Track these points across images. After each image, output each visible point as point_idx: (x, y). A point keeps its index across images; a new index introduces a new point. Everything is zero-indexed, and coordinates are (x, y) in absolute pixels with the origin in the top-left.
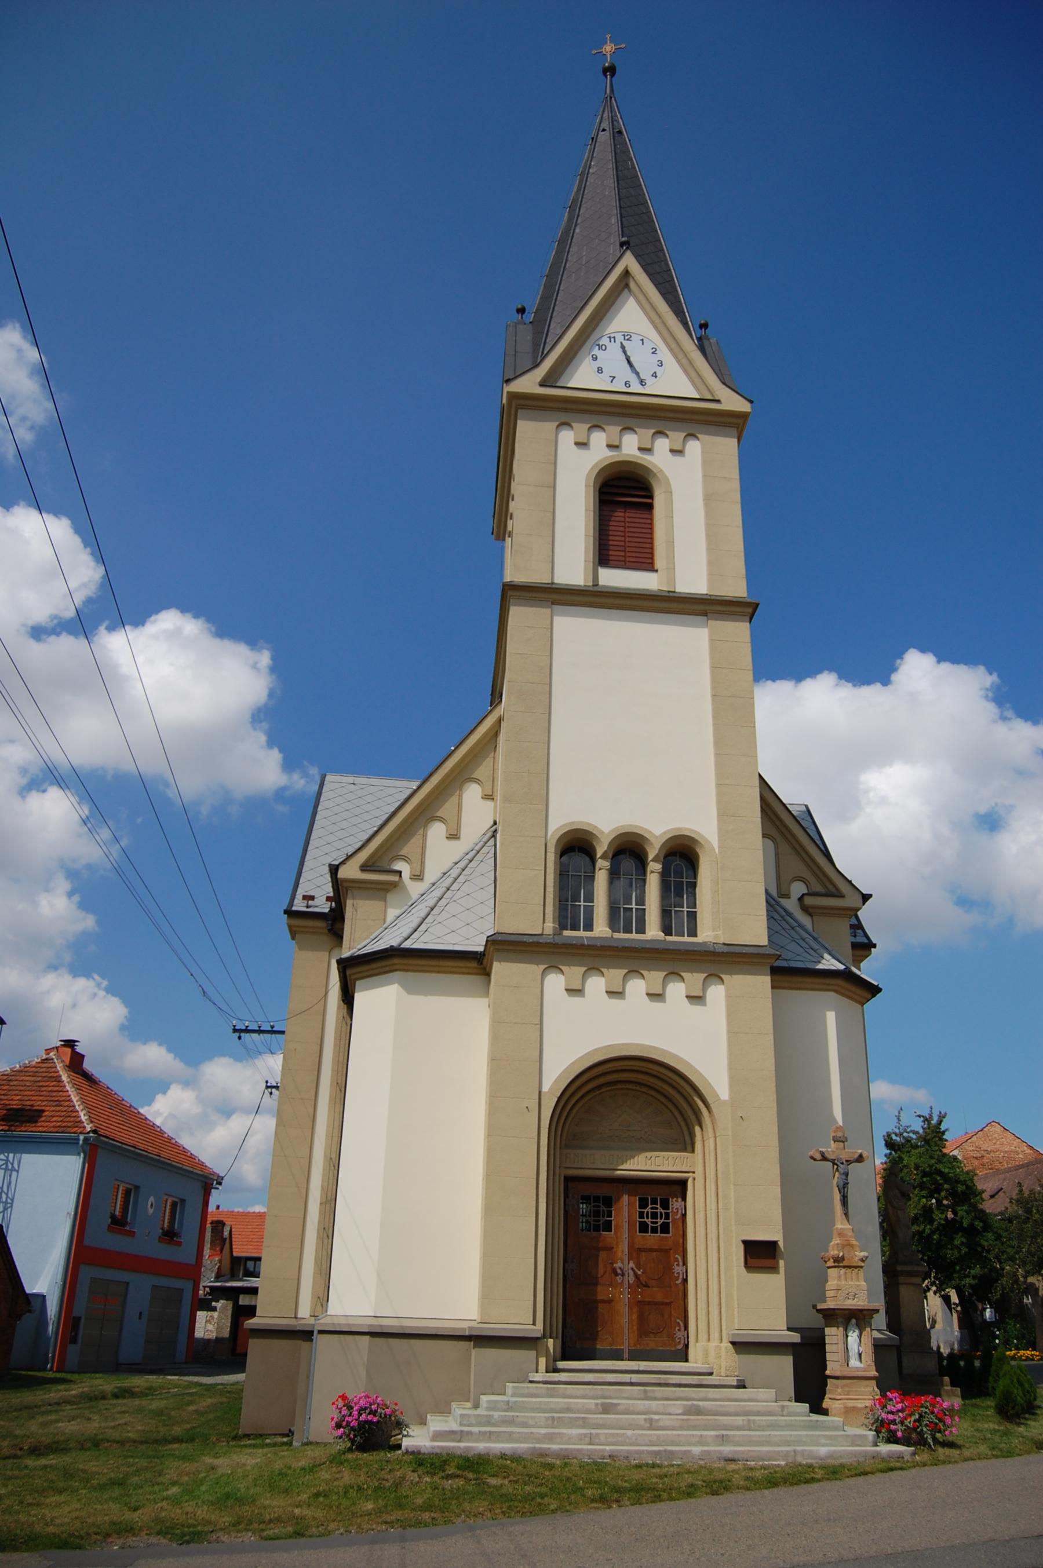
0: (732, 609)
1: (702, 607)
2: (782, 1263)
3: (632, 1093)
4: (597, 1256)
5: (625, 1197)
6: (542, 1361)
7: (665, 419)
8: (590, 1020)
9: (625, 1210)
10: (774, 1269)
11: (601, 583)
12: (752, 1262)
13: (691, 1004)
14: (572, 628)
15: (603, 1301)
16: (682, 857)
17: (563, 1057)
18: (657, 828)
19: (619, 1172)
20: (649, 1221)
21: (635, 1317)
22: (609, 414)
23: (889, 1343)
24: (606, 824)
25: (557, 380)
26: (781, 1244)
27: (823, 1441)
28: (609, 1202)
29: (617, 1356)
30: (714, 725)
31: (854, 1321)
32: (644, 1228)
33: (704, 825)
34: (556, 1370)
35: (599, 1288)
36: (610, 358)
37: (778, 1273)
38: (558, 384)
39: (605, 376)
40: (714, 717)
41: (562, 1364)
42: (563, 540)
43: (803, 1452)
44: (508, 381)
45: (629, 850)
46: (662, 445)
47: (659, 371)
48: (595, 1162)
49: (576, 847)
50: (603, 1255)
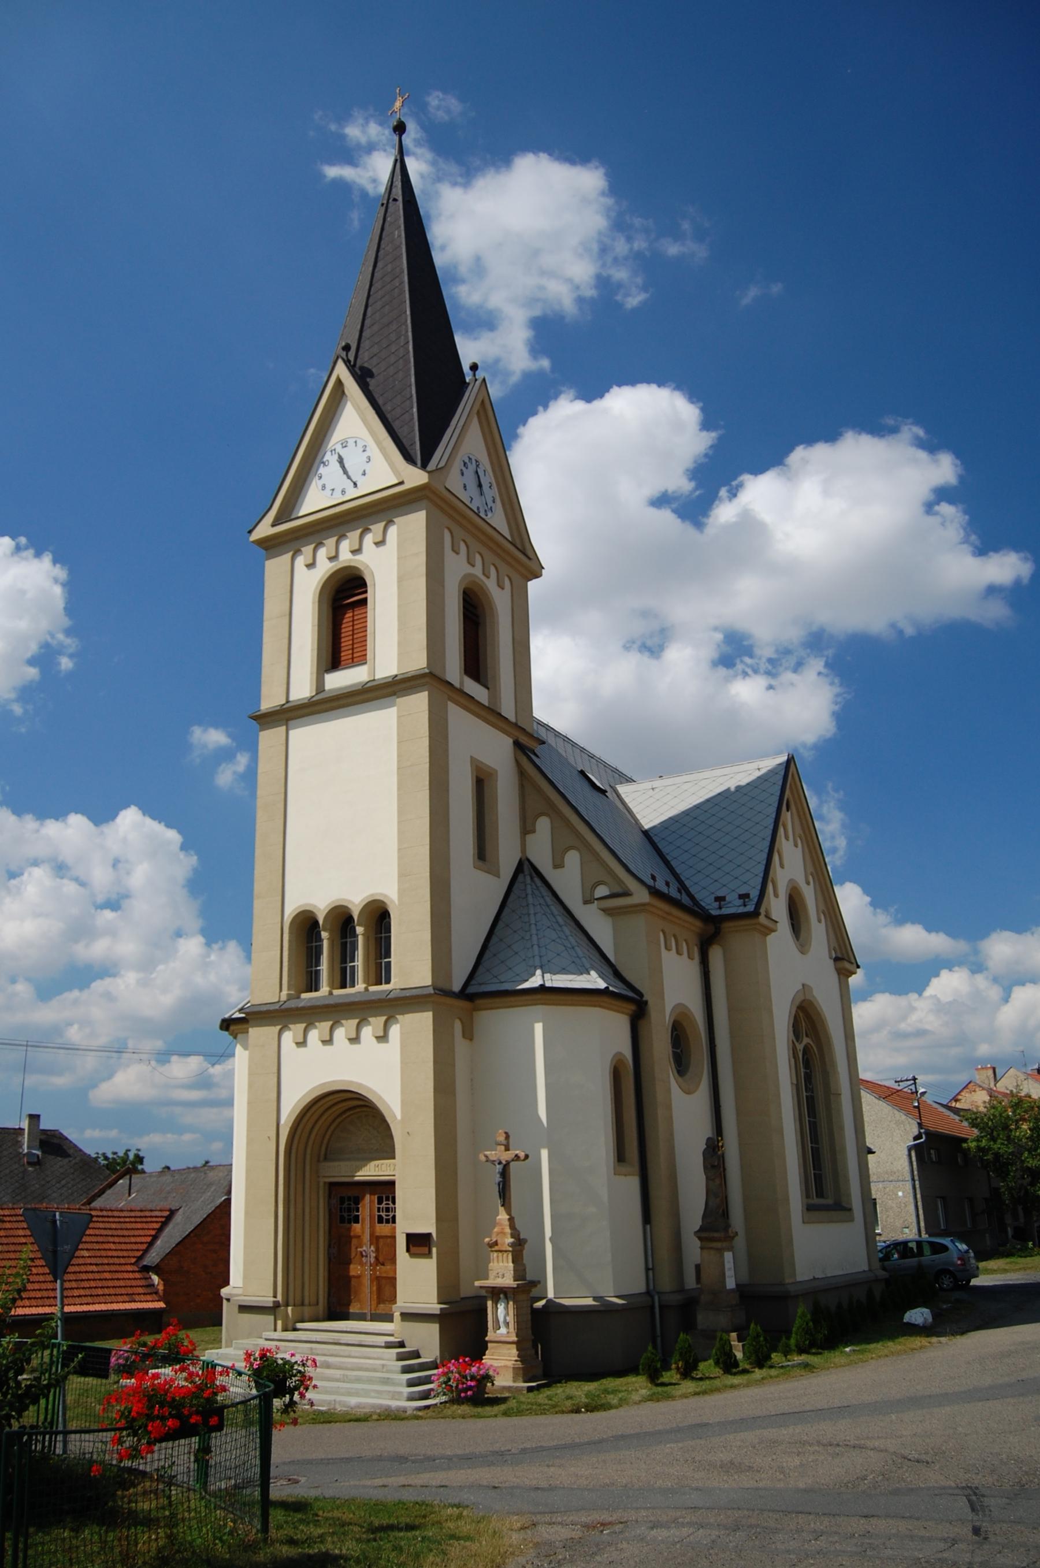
0: (412, 683)
1: (390, 690)
2: (434, 1250)
3: (341, 1121)
4: (350, 1242)
5: (368, 1197)
6: (279, 1323)
7: (318, 531)
8: (318, 1062)
9: (368, 1205)
10: (429, 1255)
11: (291, 699)
12: (413, 1249)
13: (379, 1042)
14: (307, 739)
15: (354, 1277)
16: (379, 917)
17: (295, 1096)
18: (356, 900)
19: (356, 1178)
20: (383, 1214)
21: (375, 1288)
22: (323, 530)
23: (602, 1308)
24: (321, 904)
25: (291, 514)
26: (434, 1235)
27: (373, 1394)
28: (357, 1200)
29: (362, 1317)
30: (399, 795)
31: (502, 1296)
32: (380, 1220)
33: (389, 891)
34: (295, 1329)
35: (352, 1266)
36: (329, 473)
37: (851, 1219)
38: (300, 514)
39: (328, 492)
40: (399, 789)
41: (299, 1325)
42: (293, 662)
43: (340, 1402)
44: (250, 532)
45: (343, 920)
46: (345, 546)
47: (368, 468)
48: (338, 1171)
49: (306, 927)
50: (354, 1241)
